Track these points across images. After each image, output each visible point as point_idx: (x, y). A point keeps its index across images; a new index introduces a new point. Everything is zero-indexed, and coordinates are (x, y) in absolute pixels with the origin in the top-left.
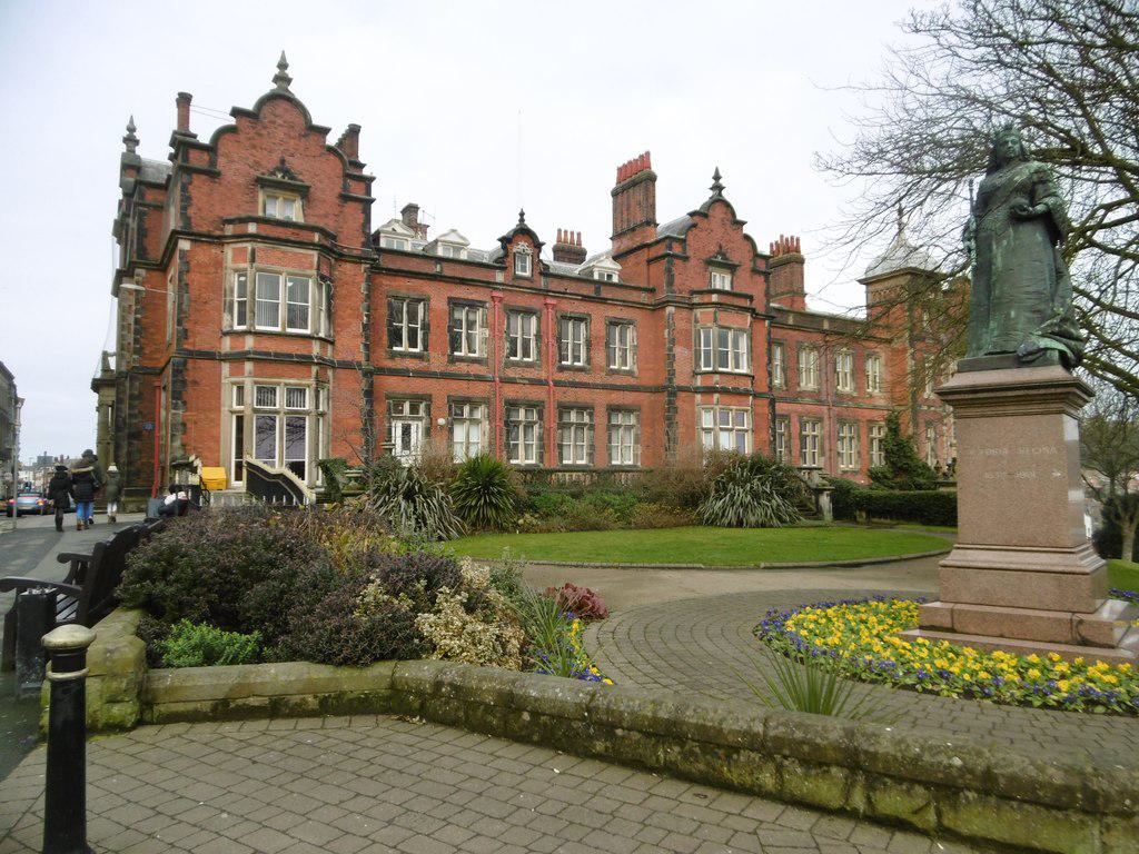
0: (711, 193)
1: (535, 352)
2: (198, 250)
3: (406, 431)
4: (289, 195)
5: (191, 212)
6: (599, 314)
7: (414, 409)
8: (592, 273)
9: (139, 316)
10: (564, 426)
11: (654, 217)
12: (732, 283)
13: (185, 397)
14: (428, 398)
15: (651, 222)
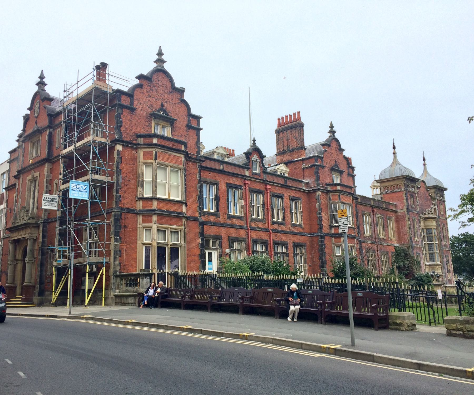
2: (126, 150)
3: (210, 254)
4: (165, 123)
5: (122, 129)
7: (214, 243)
8: (276, 172)
11: (304, 145)
12: (341, 180)
13: (121, 235)
15: (303, 148)
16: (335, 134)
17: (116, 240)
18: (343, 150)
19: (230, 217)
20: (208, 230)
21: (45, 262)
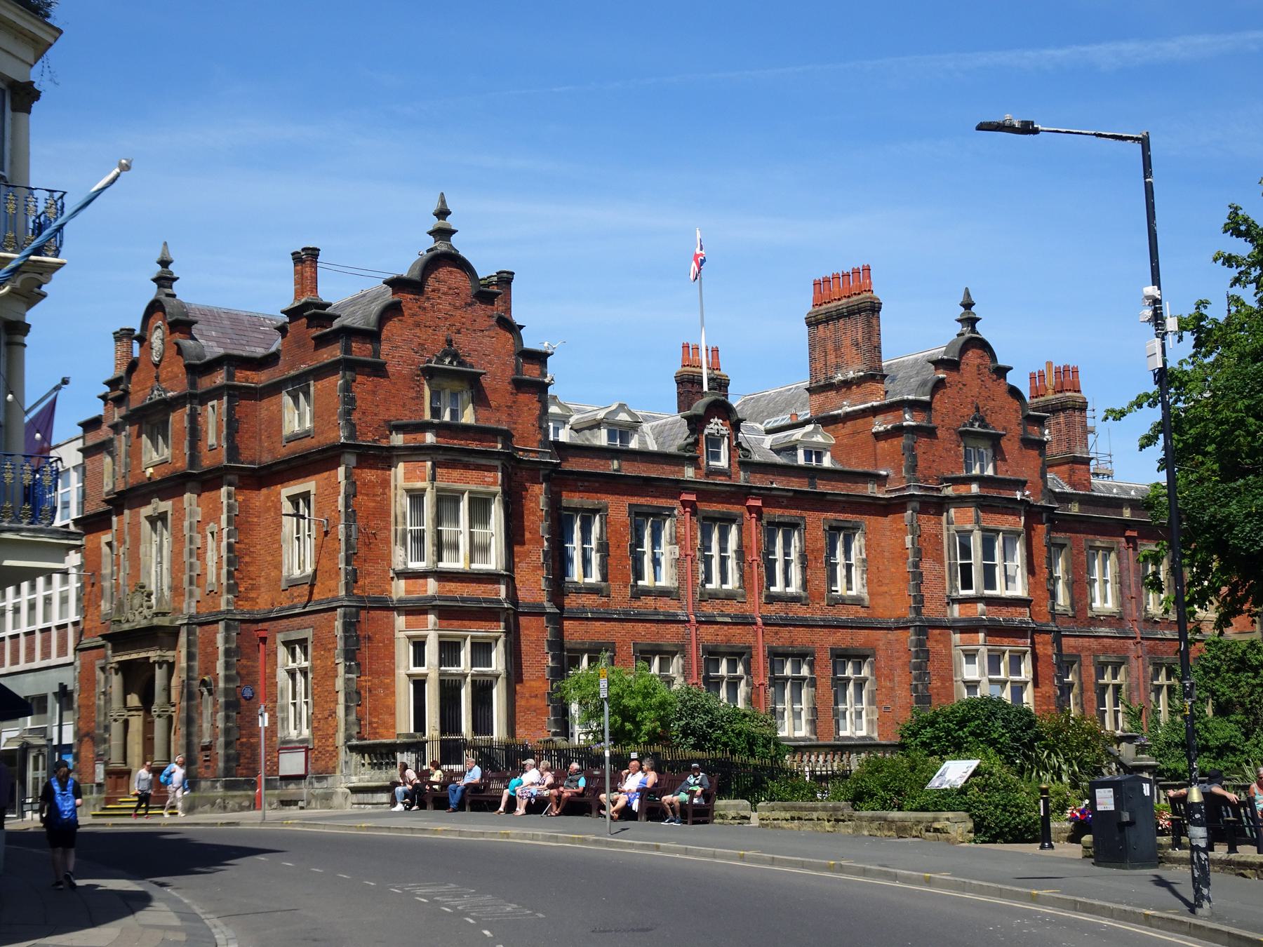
0: (959, 328)
1: (737, 576)
6: (817, 521)
9: (232, 540)
10: (778, 682)
14: (611, 647)
16: (977, 325)
17: (348, 670)
18: (1002, 372)
19: (640, 593)
20: (574, 632)
21: (196, 716)
